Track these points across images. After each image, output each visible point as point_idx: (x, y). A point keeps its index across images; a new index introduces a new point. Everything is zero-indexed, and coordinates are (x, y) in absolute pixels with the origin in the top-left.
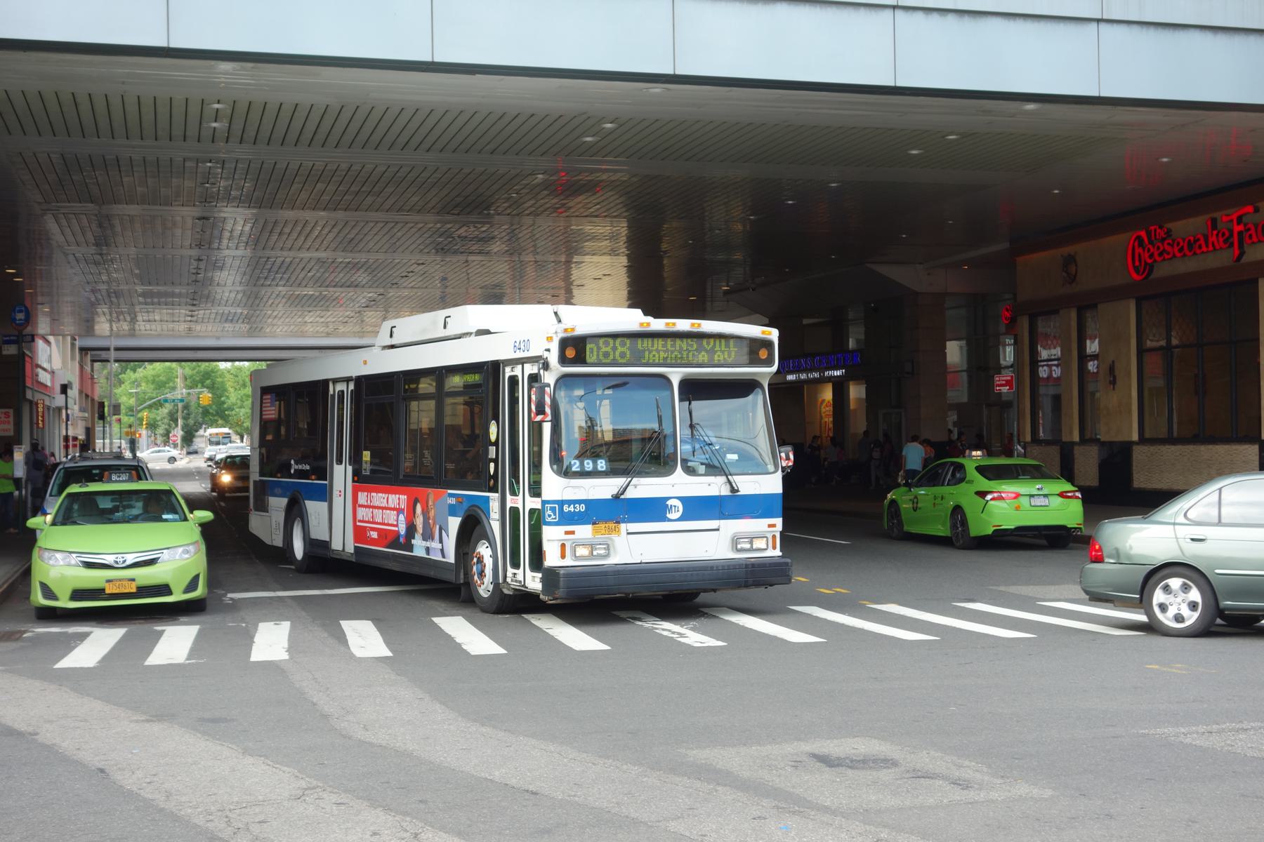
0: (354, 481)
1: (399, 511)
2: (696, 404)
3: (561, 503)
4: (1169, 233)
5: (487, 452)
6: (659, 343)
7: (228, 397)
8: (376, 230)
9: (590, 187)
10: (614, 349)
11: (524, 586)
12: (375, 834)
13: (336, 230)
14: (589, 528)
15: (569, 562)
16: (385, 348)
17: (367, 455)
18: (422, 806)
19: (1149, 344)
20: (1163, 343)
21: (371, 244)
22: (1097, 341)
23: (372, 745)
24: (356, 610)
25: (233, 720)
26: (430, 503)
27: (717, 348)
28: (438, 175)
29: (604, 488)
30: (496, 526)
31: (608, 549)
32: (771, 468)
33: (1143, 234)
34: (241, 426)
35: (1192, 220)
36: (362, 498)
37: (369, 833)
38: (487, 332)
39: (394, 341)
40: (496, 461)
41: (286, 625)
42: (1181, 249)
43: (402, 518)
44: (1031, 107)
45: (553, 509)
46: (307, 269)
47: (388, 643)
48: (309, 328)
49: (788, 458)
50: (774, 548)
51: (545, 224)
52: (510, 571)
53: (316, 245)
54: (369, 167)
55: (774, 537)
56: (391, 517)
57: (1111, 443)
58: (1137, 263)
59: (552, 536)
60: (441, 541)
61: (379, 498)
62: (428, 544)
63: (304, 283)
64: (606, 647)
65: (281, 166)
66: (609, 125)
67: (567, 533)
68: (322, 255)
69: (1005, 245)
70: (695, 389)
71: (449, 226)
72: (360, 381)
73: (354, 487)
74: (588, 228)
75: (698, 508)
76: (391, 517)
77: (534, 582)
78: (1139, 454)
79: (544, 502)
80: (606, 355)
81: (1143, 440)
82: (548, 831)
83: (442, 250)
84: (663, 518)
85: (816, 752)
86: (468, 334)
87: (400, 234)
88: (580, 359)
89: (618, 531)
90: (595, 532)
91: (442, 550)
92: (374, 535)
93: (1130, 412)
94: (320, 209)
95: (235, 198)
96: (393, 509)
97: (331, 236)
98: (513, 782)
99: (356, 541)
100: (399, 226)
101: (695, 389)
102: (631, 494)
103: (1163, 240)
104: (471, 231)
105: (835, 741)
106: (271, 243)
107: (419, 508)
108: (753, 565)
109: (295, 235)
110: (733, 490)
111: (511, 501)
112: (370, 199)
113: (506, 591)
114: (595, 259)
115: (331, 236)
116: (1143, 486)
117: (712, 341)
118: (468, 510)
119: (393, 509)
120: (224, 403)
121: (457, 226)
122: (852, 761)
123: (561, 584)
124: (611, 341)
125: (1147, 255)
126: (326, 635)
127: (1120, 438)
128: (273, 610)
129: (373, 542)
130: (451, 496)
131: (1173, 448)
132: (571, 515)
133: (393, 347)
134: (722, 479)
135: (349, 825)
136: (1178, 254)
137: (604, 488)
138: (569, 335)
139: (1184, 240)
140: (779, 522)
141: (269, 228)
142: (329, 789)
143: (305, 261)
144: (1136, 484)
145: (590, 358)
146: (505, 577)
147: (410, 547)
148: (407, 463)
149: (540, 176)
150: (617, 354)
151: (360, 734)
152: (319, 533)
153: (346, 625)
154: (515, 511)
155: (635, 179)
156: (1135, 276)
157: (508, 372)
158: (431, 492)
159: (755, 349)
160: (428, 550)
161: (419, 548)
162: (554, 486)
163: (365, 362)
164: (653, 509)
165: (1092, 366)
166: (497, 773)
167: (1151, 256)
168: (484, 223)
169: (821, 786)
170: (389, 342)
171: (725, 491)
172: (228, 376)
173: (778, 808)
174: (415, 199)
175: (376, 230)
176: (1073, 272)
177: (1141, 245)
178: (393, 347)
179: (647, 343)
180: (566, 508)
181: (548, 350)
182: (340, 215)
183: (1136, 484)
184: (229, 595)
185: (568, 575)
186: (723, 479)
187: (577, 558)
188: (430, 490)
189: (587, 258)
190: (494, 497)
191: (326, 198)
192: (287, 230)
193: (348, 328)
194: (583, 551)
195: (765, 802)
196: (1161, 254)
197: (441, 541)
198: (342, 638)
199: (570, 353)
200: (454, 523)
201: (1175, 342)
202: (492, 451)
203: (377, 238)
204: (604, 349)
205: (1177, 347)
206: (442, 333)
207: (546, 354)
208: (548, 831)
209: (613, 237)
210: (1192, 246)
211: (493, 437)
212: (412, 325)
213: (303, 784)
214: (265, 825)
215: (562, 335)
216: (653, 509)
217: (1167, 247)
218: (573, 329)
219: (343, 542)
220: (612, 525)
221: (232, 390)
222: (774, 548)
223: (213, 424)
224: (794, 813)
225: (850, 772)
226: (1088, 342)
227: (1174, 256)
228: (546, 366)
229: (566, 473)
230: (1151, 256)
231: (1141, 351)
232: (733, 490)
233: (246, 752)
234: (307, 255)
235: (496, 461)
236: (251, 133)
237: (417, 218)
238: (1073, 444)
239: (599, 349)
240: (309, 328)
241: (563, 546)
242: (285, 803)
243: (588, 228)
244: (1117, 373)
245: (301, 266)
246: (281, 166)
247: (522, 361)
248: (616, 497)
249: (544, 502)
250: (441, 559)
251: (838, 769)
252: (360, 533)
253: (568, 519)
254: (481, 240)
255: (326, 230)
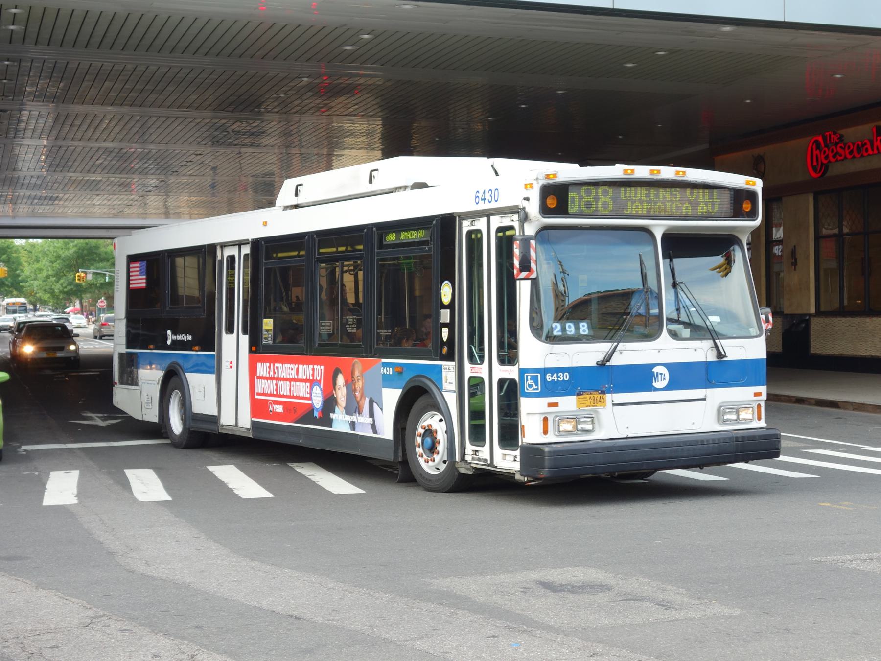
0: (251, 351)
1: (312, 382)
2: (678, 262)
3: (544, 371)
4: (841, 138)
5: (439, 316)
6: (641, 192)
7: (22, 271)
8: (158, 124)
9: (350, 90)
10: (597, 198)
11: (492, 464)
12: (156, 656)
13: (122, 123)
14: (573, 399)
15: (551, 438)
16: (286, 208)
17: (268, 324)
18: (198, 631)
19: (825, 232)
20: (836, 231)
21: (153, 137)
22: (781, 228)
23: (153, 578)
24: (139, 460)
25: (28, 558)
26: (357, 373)
27: (701, 200)
28: (214, 77)
29: (588, 355)
30: (451, 400)
31: (593, 422)
32: (754, 331)
33: (820, 139)
34: (34, 296)
35: (860, 127)
36: (262, 369)
37: (150, 655)
38: (424, 185)
39: (300, 200)
40: (450, 326)
41: (75, 474)
42: (851, 152)
43: (317, 390)
44: (727, 29)
45: (535, 379)
46: (95, 158)
47: (168, 489)
48: (96, 210)
49: (767, 321)
50: (759, 418)
51: (309, 121)
52: (470, 448)
53: (104, 136)
54: (153, 68)
55: (759, 406)
56: (303, 389)
57: (793, 316)
58: (815, 163)
59: (532, 411)
60: (372, 414)
61: (286, 369)
62: (354, 418)
63: (93, 170)
64: (362, 491)
65: (73, 65)
66: (366, 36)
67: (551, 405)
68: (109, 145)
69: (705, 146)
70: (679, 245)
71: (223, 121)
72: (256, 244)
73: (251, 358)
74: (347, 126)
75: (684, 376)
76: (303, 389)
77: (508, 461)
78: (816, 324)
79: (522, 372)
80: (588, 205)
81: (819, 313)
82: (309, 651)
83: (217, 142)
84: (650, 388)
85: (542, 579)
86: (405, 187)
87: (179, 128)
88: (562, 210)
89: (602, 402)
90: (580, 403)
91: (373, 426)
92: (279, 409)
93: (808, 289)
94: (108, 105)
95: (30, 93)
96: (306, 381)
97: (117, 129)
98: (279, 609)
99: (254, 413)
100: (180, 120)
101: (679, 245)
102: (616, 361)
103: (836, 144)
104: (244, 126)
105: (559, 570)
106: (63, 134)
107: (341, 380)
108: (743, 438)
109: (84, 127)
110: (720, 355)
111: (469, 370)
112: (153, 97)
113: (463, 471)
114: (354, 152)
115: (117, 129)
116: (818, 352)
117: (696, 191)
118: (169, 366)
119: (306, 381)
120: (18, 276)
121: (231, 122)
122: (573, 587)
123: (547, 463)
124: (593, 189)
125: (823, 156)
126: (111, 482)
127: (799, 312)
128: (64, 461)
129: (277, 416)
130: (385, 366)
131: (844, 319)
132: (553, 384)
133: (296, 206)
134: (707, 344)
135: (133, 649)
136: (848, 156)
137: (588, 355)
138: (550, 181)
139: (853, 144)
140: (763, 389)
141: (61, 121)
142: (114, 618)
143: (93, 150)
144: (813, 351)
145: (572, 209)
146: (463, 455)
147: (329, 423)
148: (324, 328)
149: (306, 79)
150: (600, 203)
151: (142, 569)
152: (203, 405)
153: (129, 473)
154: (477, 385)
155: (388, 84)
156: (814, 175)
157: (466, 226)
158: (358, 363)
159: (740, 202)
160: (353, 425)
161: (340, 422)
162: (533, 352)
163: (265, 224)
164: (638, 378)
165: (777, 250)
166: (265, 601)
167: (827, 157)
168: (256, 120)
169: (545, 608)
170: (294, 201)
171: (712, 357)
172: (22, 251)
173: (509, 628)
174: (194, 97)
175: (158, 124)
176: (762, 170)
177: (818, 148)
178: (296, 206)
179: (631, 192)
180: (549, 378)
181: (527, 199)
182: (126, 109)
183: (813, 351)
184: (24, 447)
185: (554, 454)
186: (710, 343)
187: (561, 433)
188: (356, 360)
189: (347, 152)
190: (449, 370)
191: (113, 94)
192: (77, 123)
193: (133, 210)
194: (567, 426)
195: (498, 623)
196: (834, 156)
197: (372, 414)
198: (126, 485)
199: (552, 202)
200: (391, 397)
201: (846, 230)
202: (445, 316)
203: (160, 130)
204: (586, 199)
205: (847, 234)
206: (367, 188)
207: (522, 204)
208: (309, 651)
209: (369, 134)
210: (860, 149)
211: (446, 299)
212: (315, 184)
213: (91, 613)
214: (57, 650)
215: (543, 182)
216: (638, 378)
217: (841, 151)
218: (555, 175)
219: (236, 417)
220: (597, 396)
221: (26, 264)
222: (759, 418)
223: (9, 294)
224: (523, 632)
225: (571, 596)
226: (774, 230)
227: (846, 158)
228: (525, 218)
229: (551, 339)
230: (827, 157)
231: (818, 238)
232: (720, 355)
233: (39, 585)
234: (97, 145)
235: (450, 326)
236: (45, 35)
237: (195, 113)
238: (810, 315)
239: (581, 198)
240: (96, 210)
241: (546, 420)
242: (75, 631)
243: (347, 126)
244: (798, 256)
245: (90, 154)
246: (73, 65)
247: (487, 214)
248: (602, 364)
249: (522, 372)
250: (370, 434)
251: (561, 594)
252: (258, 406)
253: (551, 389)
254: (252, 134)
255: (113, 123)
